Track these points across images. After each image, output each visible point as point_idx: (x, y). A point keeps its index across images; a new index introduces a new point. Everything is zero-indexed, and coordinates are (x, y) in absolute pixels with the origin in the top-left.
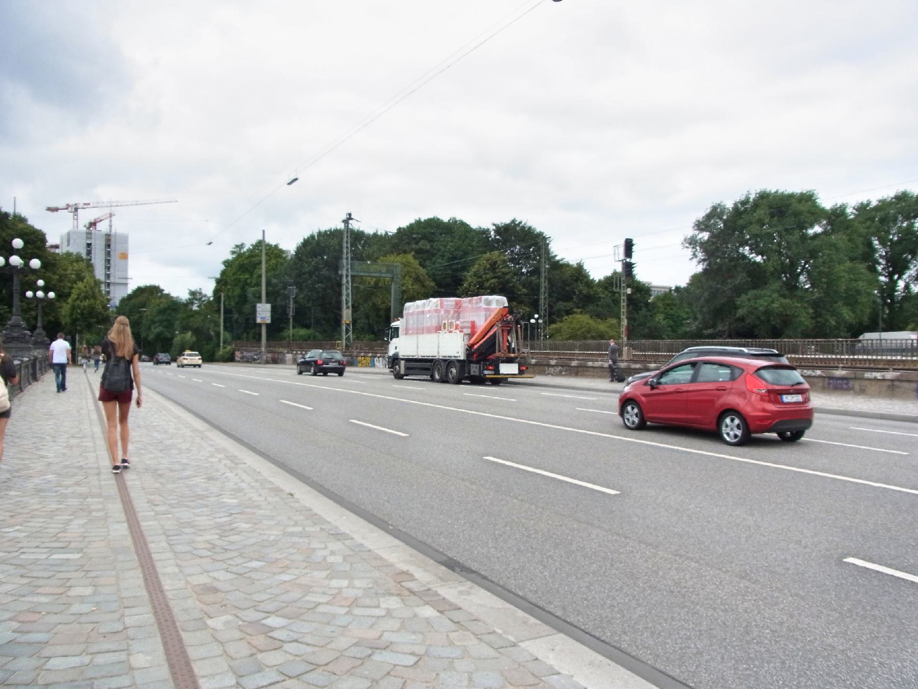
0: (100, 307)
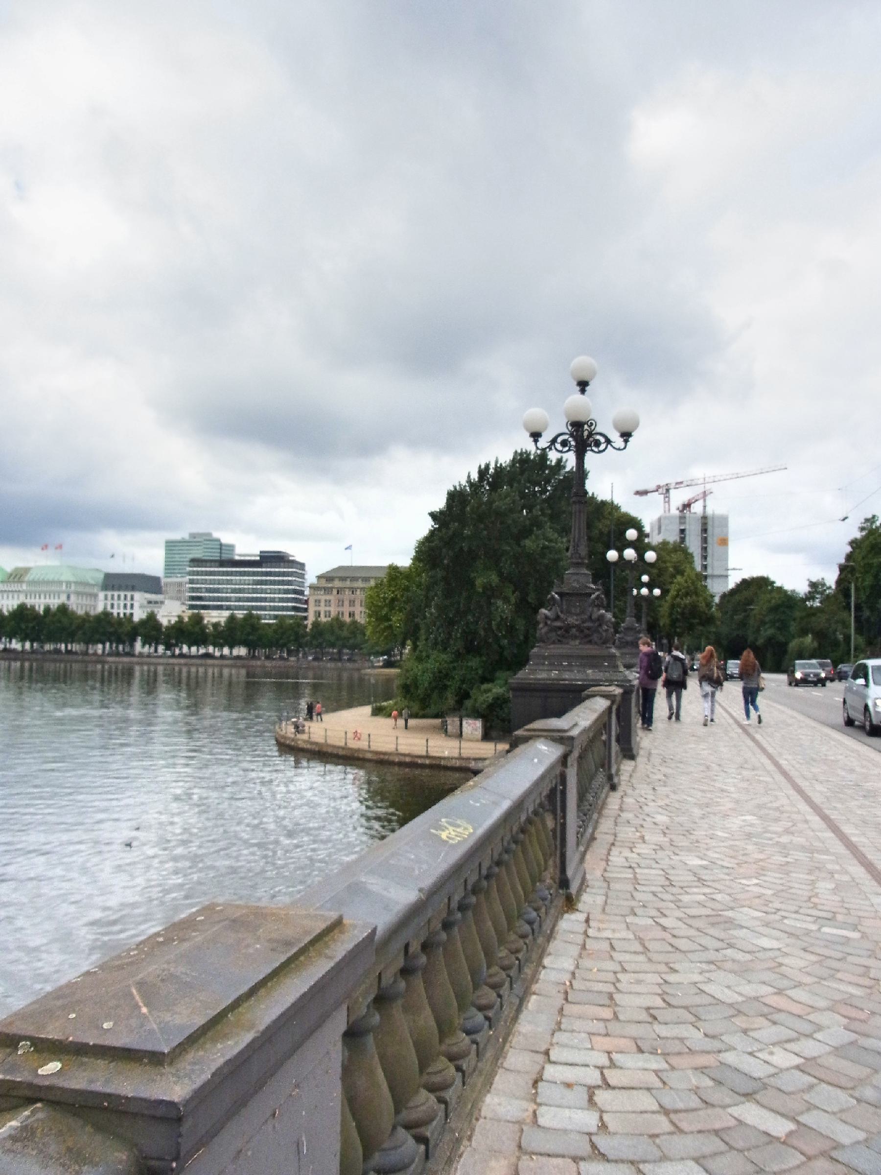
0: (703, 604)
